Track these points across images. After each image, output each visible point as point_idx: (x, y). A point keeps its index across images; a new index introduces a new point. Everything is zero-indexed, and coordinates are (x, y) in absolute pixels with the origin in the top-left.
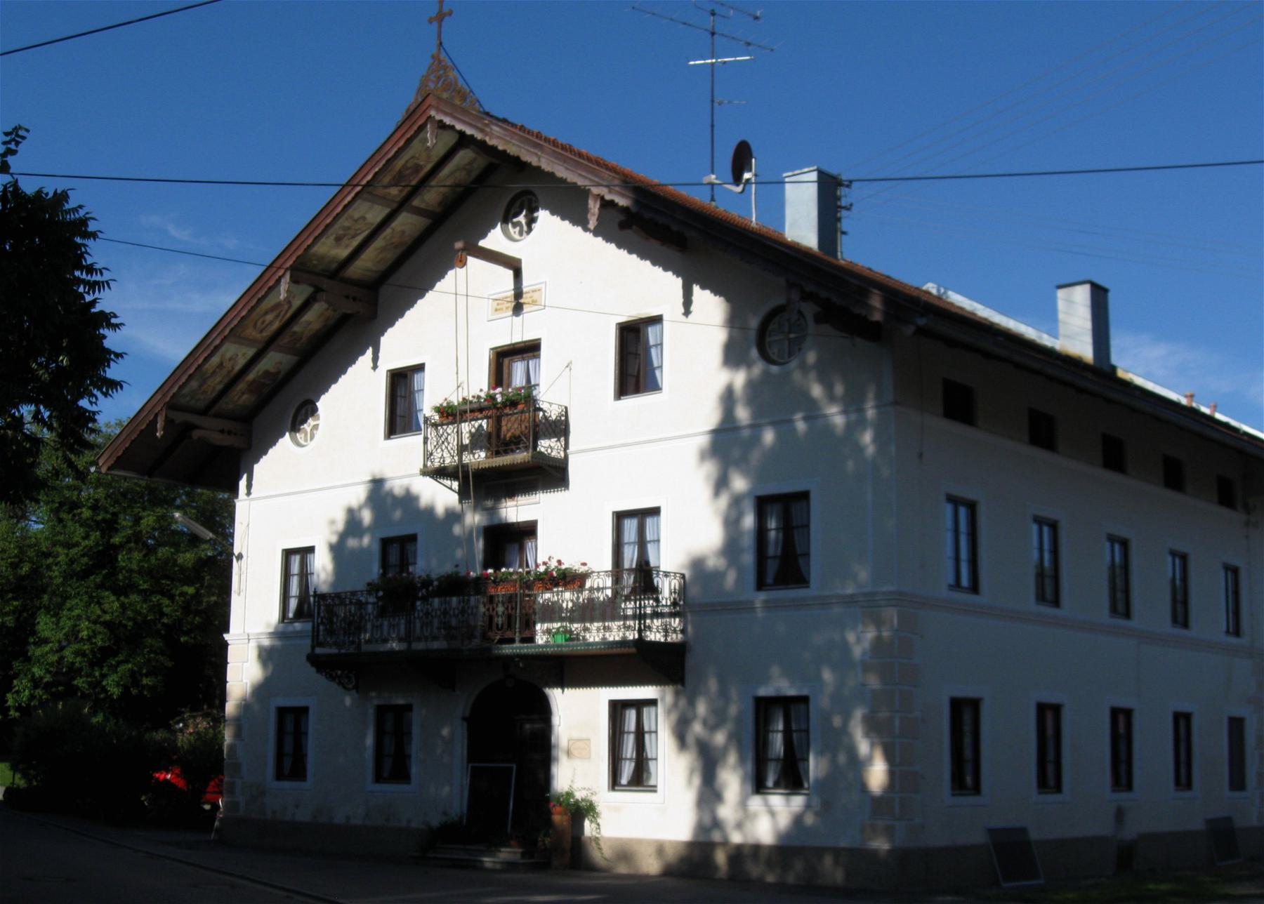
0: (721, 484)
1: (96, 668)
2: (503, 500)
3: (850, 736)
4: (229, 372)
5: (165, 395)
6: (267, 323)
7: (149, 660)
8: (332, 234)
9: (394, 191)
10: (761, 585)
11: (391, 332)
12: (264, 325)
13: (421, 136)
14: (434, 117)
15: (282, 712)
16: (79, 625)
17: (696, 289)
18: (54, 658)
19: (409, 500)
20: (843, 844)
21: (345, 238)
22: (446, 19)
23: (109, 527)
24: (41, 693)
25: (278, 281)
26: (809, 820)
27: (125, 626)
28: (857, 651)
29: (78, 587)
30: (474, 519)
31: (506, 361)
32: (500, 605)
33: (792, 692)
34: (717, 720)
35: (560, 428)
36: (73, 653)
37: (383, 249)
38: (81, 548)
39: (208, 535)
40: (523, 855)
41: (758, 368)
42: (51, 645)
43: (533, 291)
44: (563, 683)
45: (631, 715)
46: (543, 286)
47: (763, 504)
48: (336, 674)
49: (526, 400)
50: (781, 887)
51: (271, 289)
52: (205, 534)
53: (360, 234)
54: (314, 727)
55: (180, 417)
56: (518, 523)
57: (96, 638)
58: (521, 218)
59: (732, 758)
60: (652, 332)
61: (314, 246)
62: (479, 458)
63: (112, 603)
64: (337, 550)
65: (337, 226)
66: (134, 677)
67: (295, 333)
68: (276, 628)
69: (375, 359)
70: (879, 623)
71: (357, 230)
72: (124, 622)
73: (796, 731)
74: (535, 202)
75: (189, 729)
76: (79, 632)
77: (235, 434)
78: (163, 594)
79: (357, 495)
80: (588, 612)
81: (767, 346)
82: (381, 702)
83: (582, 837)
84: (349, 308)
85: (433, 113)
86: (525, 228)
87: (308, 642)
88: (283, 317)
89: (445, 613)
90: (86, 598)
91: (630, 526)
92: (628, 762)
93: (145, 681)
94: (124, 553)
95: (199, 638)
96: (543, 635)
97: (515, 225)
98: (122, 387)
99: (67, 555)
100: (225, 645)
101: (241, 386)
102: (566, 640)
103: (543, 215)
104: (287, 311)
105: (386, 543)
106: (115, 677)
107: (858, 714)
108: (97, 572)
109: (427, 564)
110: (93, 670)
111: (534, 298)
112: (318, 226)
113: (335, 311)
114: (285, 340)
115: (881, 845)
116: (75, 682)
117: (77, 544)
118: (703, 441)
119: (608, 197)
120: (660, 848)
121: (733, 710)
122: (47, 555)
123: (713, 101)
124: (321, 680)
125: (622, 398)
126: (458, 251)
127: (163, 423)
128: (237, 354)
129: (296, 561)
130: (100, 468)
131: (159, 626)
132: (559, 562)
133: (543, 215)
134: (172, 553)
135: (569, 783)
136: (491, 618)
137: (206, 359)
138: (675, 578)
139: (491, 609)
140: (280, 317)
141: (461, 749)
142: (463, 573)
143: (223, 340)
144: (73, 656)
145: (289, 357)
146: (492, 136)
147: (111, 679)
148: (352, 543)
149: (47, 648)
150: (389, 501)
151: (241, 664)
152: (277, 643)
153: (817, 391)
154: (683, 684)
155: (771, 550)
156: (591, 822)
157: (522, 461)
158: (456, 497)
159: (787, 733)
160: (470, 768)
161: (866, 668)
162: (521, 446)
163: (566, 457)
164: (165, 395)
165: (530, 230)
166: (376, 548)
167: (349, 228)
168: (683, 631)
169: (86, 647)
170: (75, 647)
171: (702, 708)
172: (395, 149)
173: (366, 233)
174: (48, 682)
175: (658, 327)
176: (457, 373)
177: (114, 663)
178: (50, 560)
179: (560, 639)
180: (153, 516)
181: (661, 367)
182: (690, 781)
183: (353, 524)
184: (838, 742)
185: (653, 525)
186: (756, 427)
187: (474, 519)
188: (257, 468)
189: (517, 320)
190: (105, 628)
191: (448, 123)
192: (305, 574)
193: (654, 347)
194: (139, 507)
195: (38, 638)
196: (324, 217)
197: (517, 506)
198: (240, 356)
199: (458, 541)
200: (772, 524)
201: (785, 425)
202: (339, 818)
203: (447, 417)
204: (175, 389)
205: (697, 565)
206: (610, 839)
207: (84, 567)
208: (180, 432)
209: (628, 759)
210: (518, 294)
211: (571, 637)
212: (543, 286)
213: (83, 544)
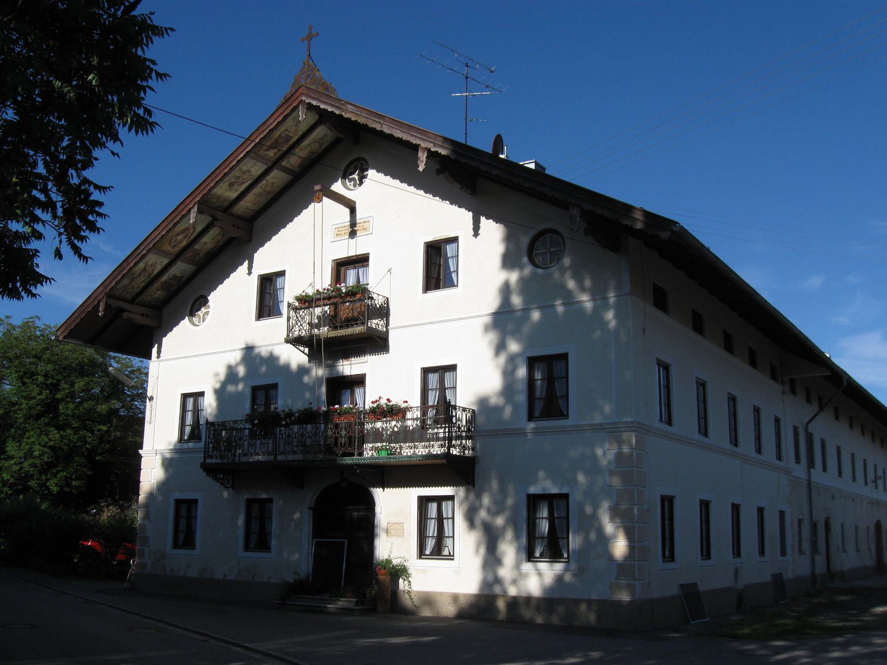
0: (500, 347)
1: (43, 475)
2: (341, 360)
3: (599, 520)
4: (150, 274)
5: (105, 288)
6: (178, 241)
7: (77, 470)
8: (227, 181)
9: (271, 153)
10: (531, 418)
11: (170, 335)
12: (176, 243)
13: (294, 115)
14: (304, 101)
15: (179, 503)
16: (34, 448)
17: (483, 219)
18: (16, 468)
19: (272, 359)
20: (594, 596)
21: (235, 185)
22: (314, 39)
23: (55, 388)
24: (7, 490)
25: (189, 211)
26: (568, 578)
27: (62, 449)
28: (604, 462)
29: (34, 424)
30: (319, 372)
31: (343, 269)
32: (343, 430)
33: (555, 491)
34: (498, 508)
35: (384, 312)
36: (29, 465)
37: (259, 195)
38: (36, 400)
39: (131, 383)
40: (357, 604)
41: (528, 270)
42: (15, 460)
43: (364, 222)
44: (383, 485)
45: (433, 507)
46: (371, 218)
47: (532, 362)
48: (219, 476)
49: (360, 292)
50: (546, 627)
51: (183, 216)
52: (129, 382)
53: (246, 182)
54: (201, 511)
55: (115, 303)
56: (351, 376)
57: (43, 456)
58: (356, 176)
59: (509, 535)
60: (450, 249)
61: (215, 188)
62: (324, 331)
63: (55, 434)
64: (220, 393)
65: (231, 175)
66: (68, 481)
67: (196, 249)
68: (175, 445)
69: (250, 268)
70: (620, 442)
71: (244, 179)
72: (62, 446)
73: (558, 518)
74: (366, 165)
75: (108, 513)
76: (33, 452)
77: (151, 317)
78: (86, 430)
79: (235, 357)
80: (405, 435)
81: (534, 257)
82: (249, 496)
83: (398, 591)
84: (235, 233)
85: (304, 98)
86: (358, 182)
87: (202, 455)
88: (189, 238)
89: (302, 435)
90: (38, 431)
91: (433, 378)
92: (430, 539)
93: (74, 483)
94: (64, 404)
95: (108, 458)
96: (369, 452)
97: (350, 180)
98: (99, 232)
99: (27, 404)
100: (140, 457)
101: (157, 285)
102: (388, 455)
103: (372, 173)
104: (192, 234)
105: (255, 390)
106: (55, 480)
107: (605, 505)
108: (47, 415)
109: (283, 403)
110: (41, 476)
111: (365, 227)
112: (219, 175)
113: (223, 235)
114: (188, 254)
115: (625, 597)
116: (30, 483)
117: (34, 398)
118: (488, 319)
119: (433, 149)
120: (455, 598)
121: (510, 502)
122: (14, 404)
123: (466, 119)
124: (209, 480)
125: (428, 292)
126: (317, 192)
127: (104, 307)
128: (157, 262)
129: (190, 402)
130: (58, 337)
131: (84, 449)
132: (389, 400)
133: (372, 173)
134: (94, 405)
135: (389, 553)
136: (336, 438)
137: (136, 264)
138: (469, 413)
139: (336, 432)
140: (187, 238)
141: (307, 528)
142: (315, 408)
143: (148, 251)
144: (29, 467)
145: (190, 266)
146: (346, 111)
147: (52, 482)
148: (230, 388)
149: (13, 462)
150: (258, 360)
151: (150, 470)
152: (176, 456)
153: (571, 284)
154: (474, 486)
155: (538, 393)
156: (404, 580)
157: (360, 332)
158: (307, 358)
159: (551, 519)
160: (314, 542)
161: (611, 473)
162: (358, 322)
163: (387, 331)
164: (105, 288)
165: (361, 183)
166: (248, 392)
167: (239, 178)
168: (473, 449)
169: (37, 462)
170: (30, 461)
171: (486, 500)
172: (276, 122)
173: (249, 182)
174: (12, 483)
175: (455, 245)
176: (314, 273)
177: (54, 472)
178: (17, 407)
179: (384, 454)
180: (82, 382)
181: (457, 271)
182: (477, 551)
183: (231, 376)
184: (591, 523)
185: (450, 377)
186: (526, 310)
187: (319, 372)
188: (165, 340)
189: (352, 241)
190: (50, 450)
191: (314, 104)
192: (197, 411)
193: (451, 259)
194: (74, 376)
195: (7, 455)
196: (223, 168)
197: (343, 365)
198: (158, 263)
199: (307, 387)
200: (538, 376)
201: (547, 308)
202: (219, 576)
203: (305, 303)
204: (113, 284)
205: (483, 402)
206: (419, 592)
207: (38, 412)
208: (114, 314)
209: (431, 537)
210: (353, 224)
211: (391, 453)
212: (371, 218)
213: (38, 397)
